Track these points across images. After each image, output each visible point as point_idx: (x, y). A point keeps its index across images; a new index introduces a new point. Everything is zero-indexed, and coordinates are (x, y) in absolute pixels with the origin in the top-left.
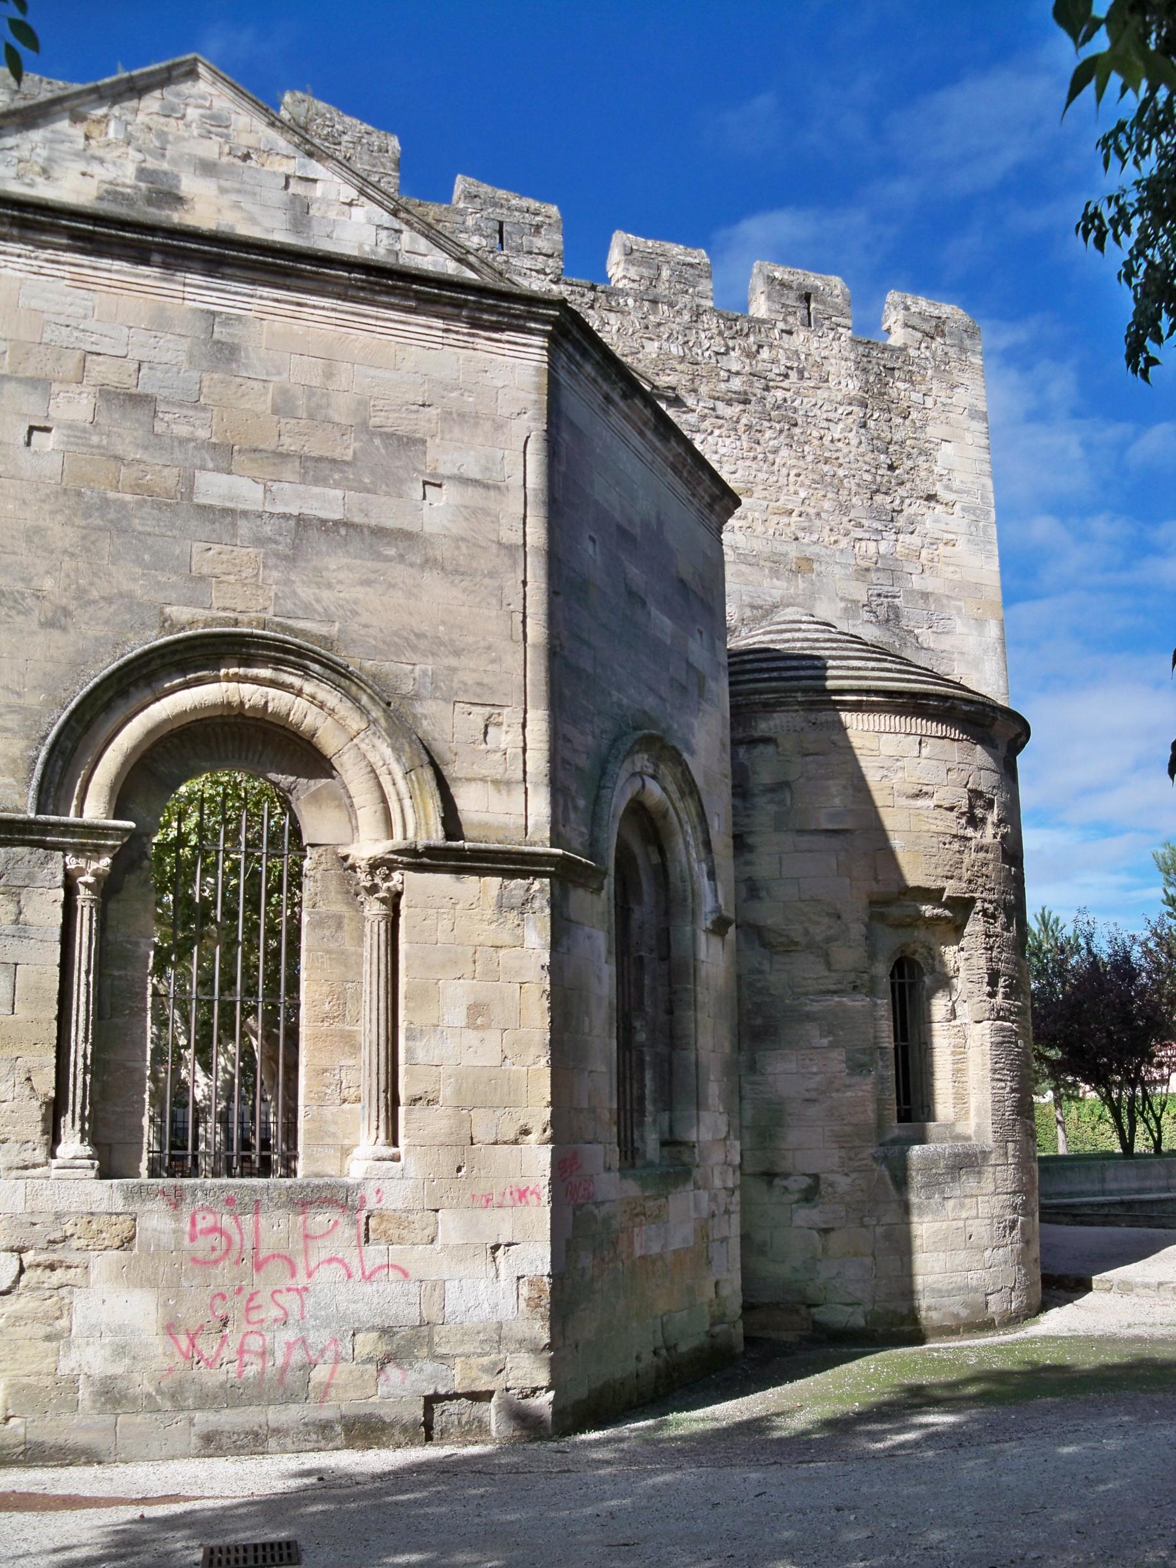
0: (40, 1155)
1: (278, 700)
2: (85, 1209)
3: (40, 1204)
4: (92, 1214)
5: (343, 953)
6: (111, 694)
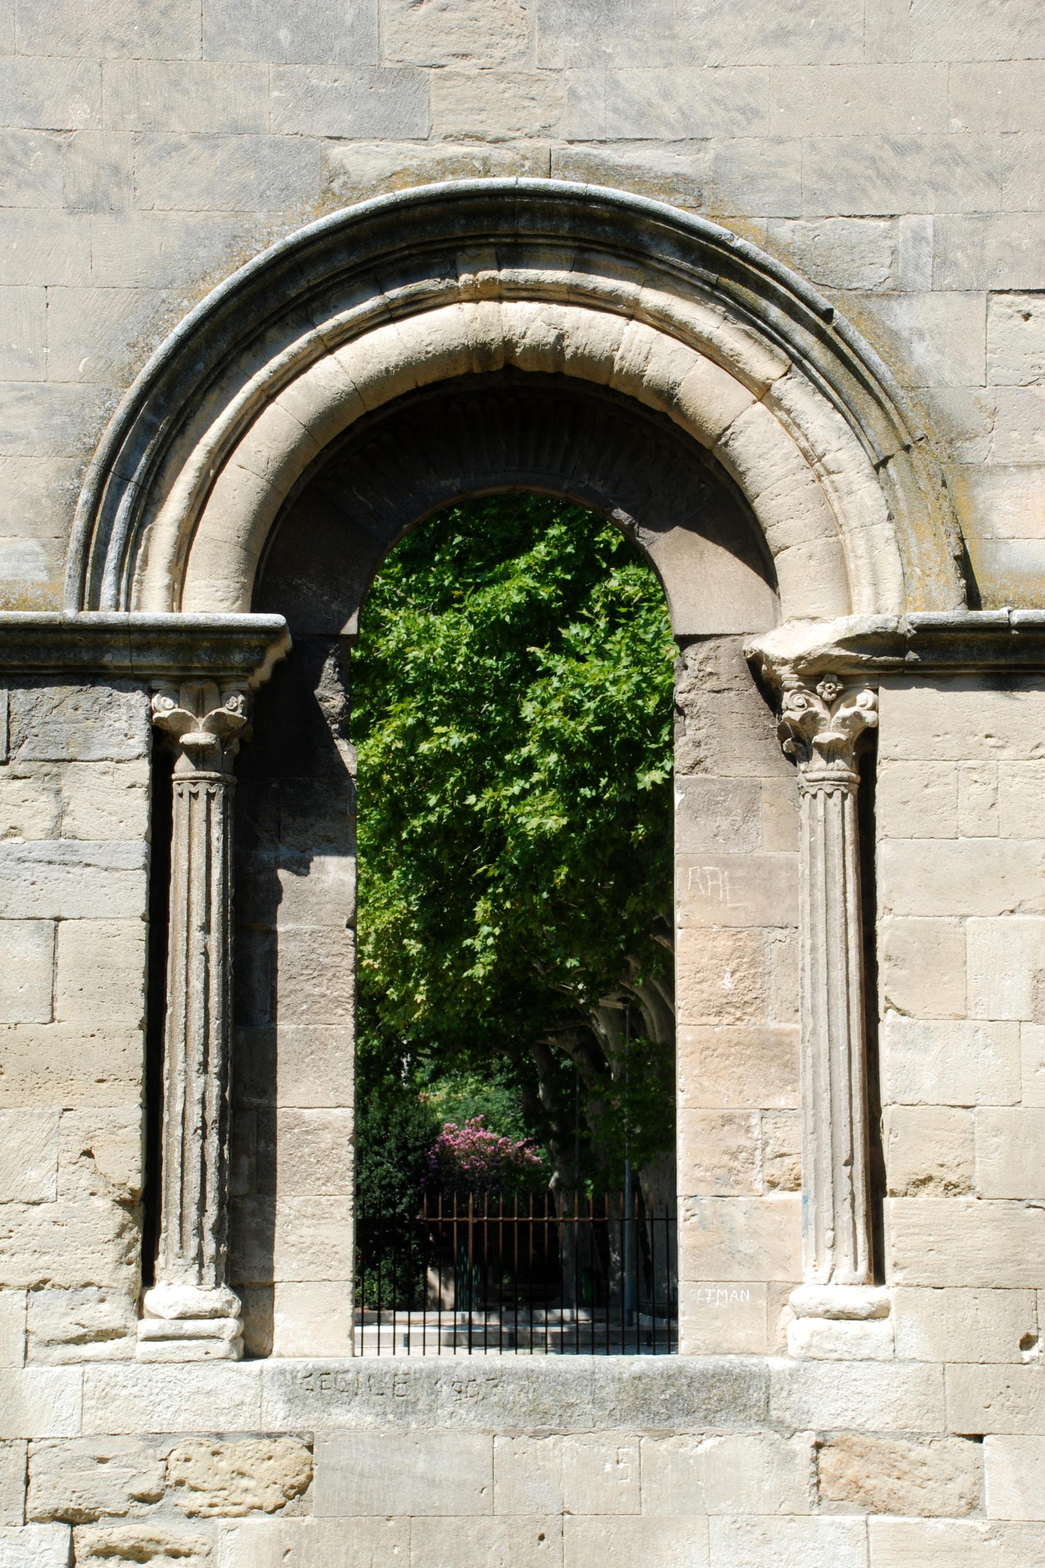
0: (112, 1313)
1: (590, 330)
2: (209, 1426)
3: (110, 1418)
4: (220, 1436)
5: (759, 866)
6: (223, 346)
